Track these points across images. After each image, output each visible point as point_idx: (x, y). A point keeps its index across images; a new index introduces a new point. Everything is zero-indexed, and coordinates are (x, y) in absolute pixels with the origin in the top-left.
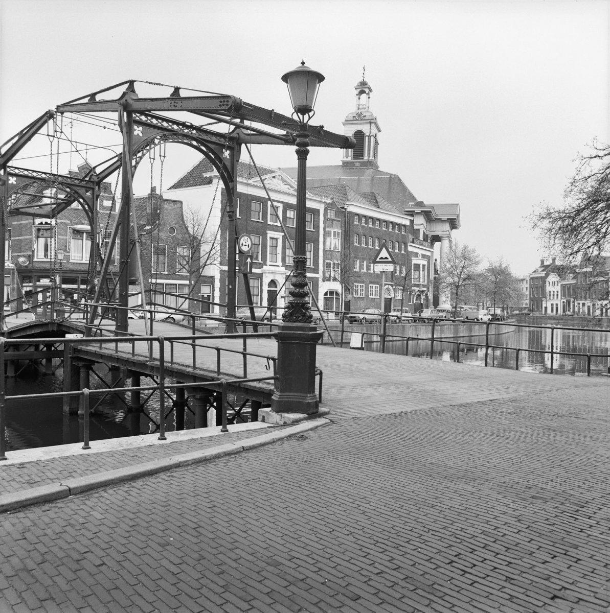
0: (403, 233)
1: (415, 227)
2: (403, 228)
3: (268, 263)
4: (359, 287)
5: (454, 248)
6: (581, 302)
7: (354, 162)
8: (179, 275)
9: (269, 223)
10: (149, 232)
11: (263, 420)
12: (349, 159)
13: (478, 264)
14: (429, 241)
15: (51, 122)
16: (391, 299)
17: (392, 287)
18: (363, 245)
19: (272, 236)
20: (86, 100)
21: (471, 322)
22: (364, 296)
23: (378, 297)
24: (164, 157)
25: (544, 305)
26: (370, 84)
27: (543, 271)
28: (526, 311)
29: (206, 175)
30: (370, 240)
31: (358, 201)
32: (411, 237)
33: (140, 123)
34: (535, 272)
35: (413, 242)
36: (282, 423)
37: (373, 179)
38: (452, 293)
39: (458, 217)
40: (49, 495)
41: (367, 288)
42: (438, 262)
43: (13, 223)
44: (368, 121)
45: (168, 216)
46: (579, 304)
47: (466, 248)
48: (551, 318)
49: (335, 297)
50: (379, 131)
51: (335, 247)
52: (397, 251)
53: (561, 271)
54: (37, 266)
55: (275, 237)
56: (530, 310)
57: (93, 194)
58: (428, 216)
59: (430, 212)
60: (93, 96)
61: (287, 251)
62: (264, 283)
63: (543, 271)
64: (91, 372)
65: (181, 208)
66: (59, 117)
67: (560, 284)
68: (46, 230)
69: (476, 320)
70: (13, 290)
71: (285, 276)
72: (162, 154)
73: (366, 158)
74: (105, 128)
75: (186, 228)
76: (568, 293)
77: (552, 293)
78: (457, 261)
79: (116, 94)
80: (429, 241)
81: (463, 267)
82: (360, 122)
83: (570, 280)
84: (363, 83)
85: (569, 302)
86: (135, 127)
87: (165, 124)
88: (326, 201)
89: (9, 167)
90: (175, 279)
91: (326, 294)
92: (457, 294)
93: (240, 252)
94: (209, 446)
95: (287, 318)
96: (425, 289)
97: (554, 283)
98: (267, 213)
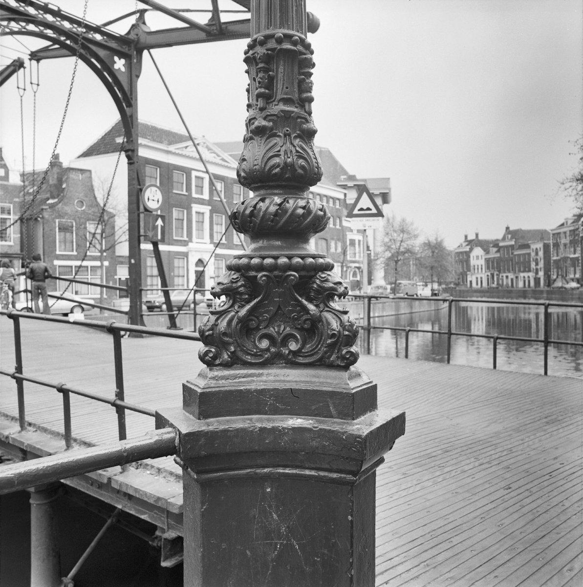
0: (338, 207)
6: (504, 275)
9: (194, 195)
10: (52, 206)
13: (417, 237)
19: (198, 210)
21: (412, 298)
25: (469, 279)
27: (467, 245)
28: (452, 285)
32: (345, 212)
34: (563, 225)
45: (74, 187)
46: (502, 276)
47: (404, 220)
48: (477, 291)
53: (485, 245)
55: (202, 211)
56: (455, 284)
63: (467, 245)
65: (91, 177)
67: (484, 258)
69: (415, 296)
75: (95, 198)
76: (492, 266)
77: (476, 267)
78: (395, 235)
81: (402, 241)
83: (493, 254)
85: (493, 275)
93: (146, 210)
95: (225, 346)
97: (477, 257)
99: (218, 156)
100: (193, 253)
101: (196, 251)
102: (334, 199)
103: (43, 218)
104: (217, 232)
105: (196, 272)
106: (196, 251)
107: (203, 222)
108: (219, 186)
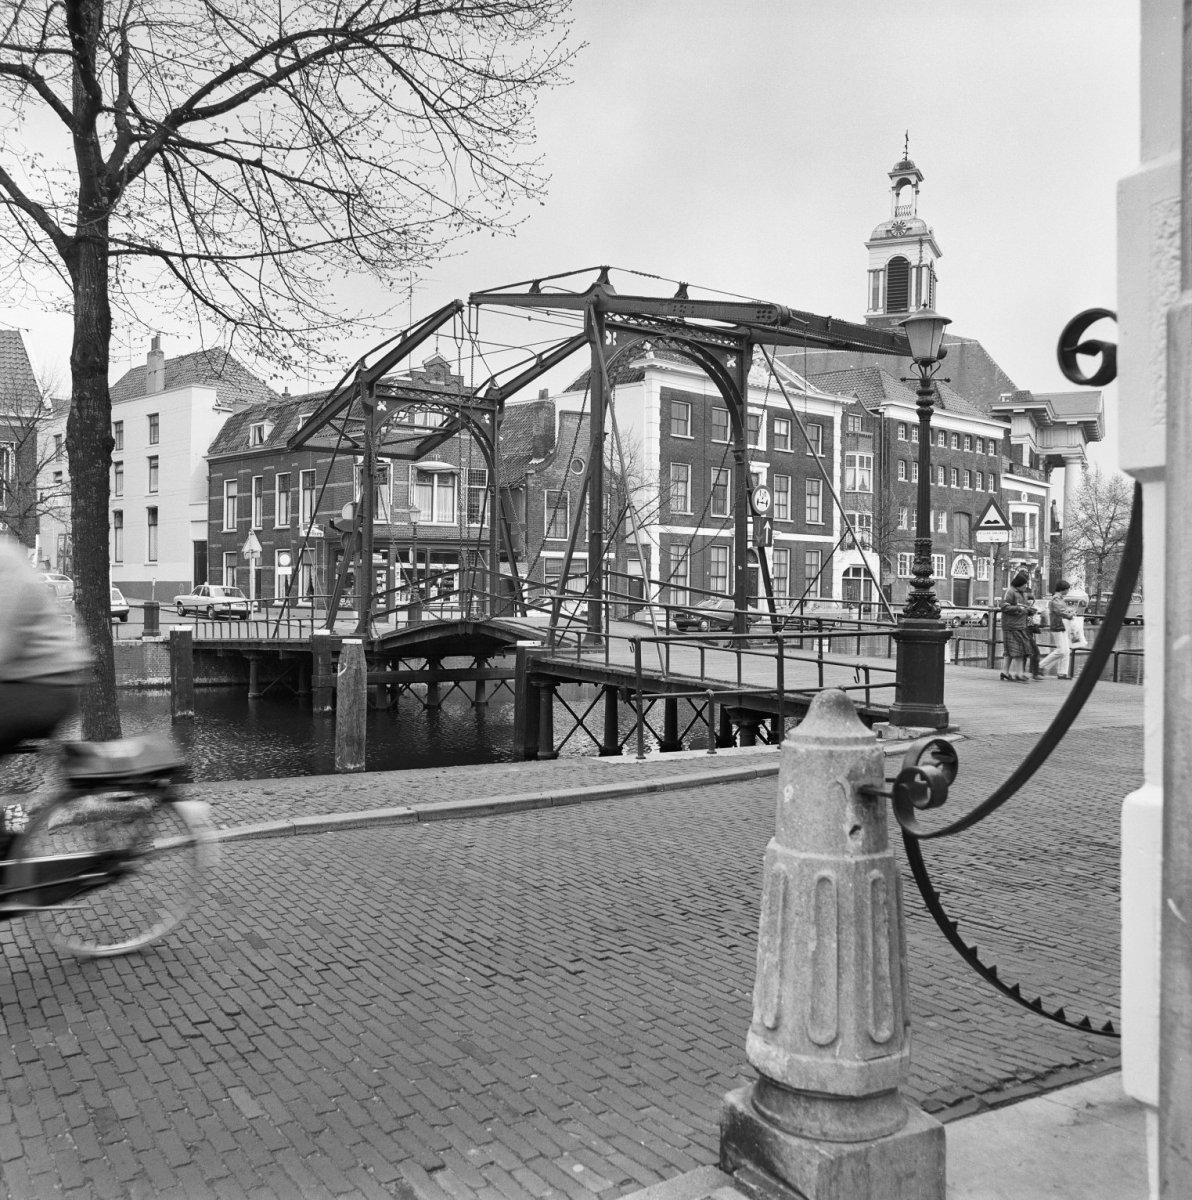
0: (991, 455)
1: (1014, 441)
2: (991, 445)
5: (1092, 481)
7: (888, 318)
10: (539, 469)
12: (880, 312)
14: (1041, 467)
16: (968, 581)
17: (971, 557)
26: (918, 165)
29: (635, 365)
32: (1006, 462)
33: (613, 327)
35: (1011, 471)
38: (1088, 566)
39: (1099, 418)
42: (1059, 508)
43: (319, 461)
44: (917, 238)
49: (862, 578)
50: (938, 255)
51: (863, 486)
52: (979, 489)
57: (492, 419)
58: (1040, 420)
59: (1044, 410)
60: (536, 283)
70: (320, 572)
74: (529, 319)
80: (1041, 467)
81: (1112, 518)
82: (899, 240)
88: (846, 401)
91: (846, 573)
92: (1100, 571)
96: (1036, 561)
103: (527, 488)
104: (779, 505)
108: (781, 428)
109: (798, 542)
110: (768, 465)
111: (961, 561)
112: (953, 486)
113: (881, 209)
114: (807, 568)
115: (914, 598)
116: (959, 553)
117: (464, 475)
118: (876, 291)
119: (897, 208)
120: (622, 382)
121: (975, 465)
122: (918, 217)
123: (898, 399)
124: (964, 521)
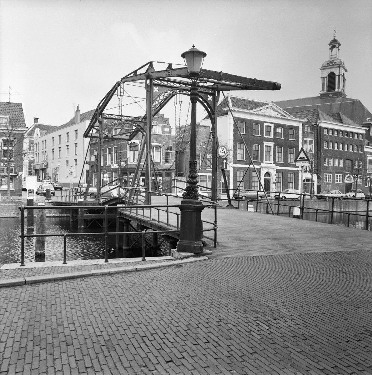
0: (360, 139)
3: (264, 161)
4: (328, 176)
8: (208, 170)
9: (265, 136)
11: (172, 256)
12: (325, 92)
15: (119, 88)
16: (351, 184)
18: (330, 148)
19: (267, 145)
20: (132, 75)
22: (331, 182)
23: (342, 182)
24: (182, 101)
30: (336, 145)
31: (326, 120)
35: (368, 145)
36: (179, 258)
37: (341, 104)
40: (14, 283)
41: (333, 177)
50: (346, 71)
52: (355, 151)
54: (130, 166)
61: (277, 154)
62: (261, 174)
64: (129, 226)
66: (122, 85)
68: (134, 146)
71: (275, 170)
72: (181, 100)
73: (336, 90)
79: (143, 71)
84: (335, 41)
86: (154, 87)
87: (172, 84)
88: (303, 121)
89: (104, 114)
90: (206, 173)
93: (220, 157)
94: (116, 267)
98: (263, 130)
99: (279, 113)
100: (263, 169)
101: (265, 168)
102: (358, 134)
103: (186, 151)
105: (265, 179)
106: (265, 168)
107: (270, 151)
108: (279, 130)
109: (285, 170)
110: (274, 143)
111: (348, 177)
112: (346, 150)
113: (326, 56)
114: (289, 179)
115: (187, 189)
116: (347, 174)
117: (164, 148)
118: (323, 84)
119: (331, 55)
120: (219, 116)
121: (354, 143)
122: (339, 58)
123: (324, 120)
124: (350, 162)
